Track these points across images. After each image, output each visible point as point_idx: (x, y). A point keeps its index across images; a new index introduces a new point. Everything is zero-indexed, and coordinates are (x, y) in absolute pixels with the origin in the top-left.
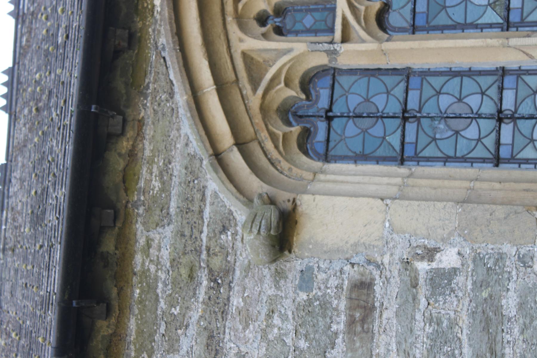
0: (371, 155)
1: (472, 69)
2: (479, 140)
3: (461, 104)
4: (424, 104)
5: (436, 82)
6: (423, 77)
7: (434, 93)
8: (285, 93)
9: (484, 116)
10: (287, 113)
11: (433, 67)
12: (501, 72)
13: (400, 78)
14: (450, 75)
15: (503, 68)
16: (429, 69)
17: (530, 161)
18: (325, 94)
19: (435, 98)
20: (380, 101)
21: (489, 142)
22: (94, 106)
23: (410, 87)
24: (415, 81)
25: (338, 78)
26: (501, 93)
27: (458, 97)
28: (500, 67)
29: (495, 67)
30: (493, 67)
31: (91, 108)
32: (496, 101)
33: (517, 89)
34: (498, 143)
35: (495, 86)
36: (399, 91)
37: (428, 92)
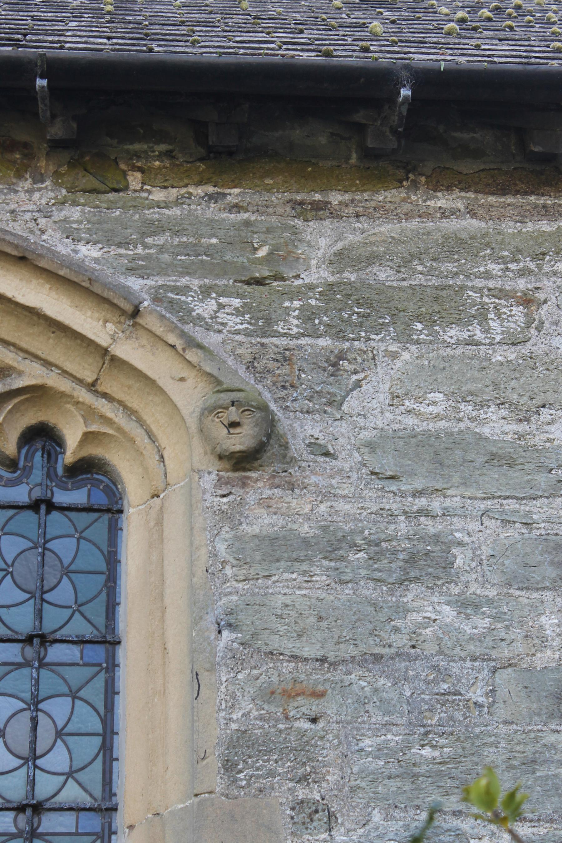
1: (117, 668)
4: (53, 671)
5: (95, 691)
6: (105, 665)
7: (74, 689)
9: (42, 264)
11: (121, 611)
12: (108, 805)
13: (98, 791)
14: (105, 715)
15: (116, 810)
16: (121, 529)
18: (78, 497)
19: (66, 690)
22: (45, 82)
23: (82, 814)
24: (97, 653)
25: (106, 517)
26: (71, 809)
27: (66, 730)
28: (117, 805)
29: (118, 792)
30: (121, 626)
31: (42, 77)
32: (58, 799)
33: (77, 834)
36: (72, 793)
37: (76, 675)
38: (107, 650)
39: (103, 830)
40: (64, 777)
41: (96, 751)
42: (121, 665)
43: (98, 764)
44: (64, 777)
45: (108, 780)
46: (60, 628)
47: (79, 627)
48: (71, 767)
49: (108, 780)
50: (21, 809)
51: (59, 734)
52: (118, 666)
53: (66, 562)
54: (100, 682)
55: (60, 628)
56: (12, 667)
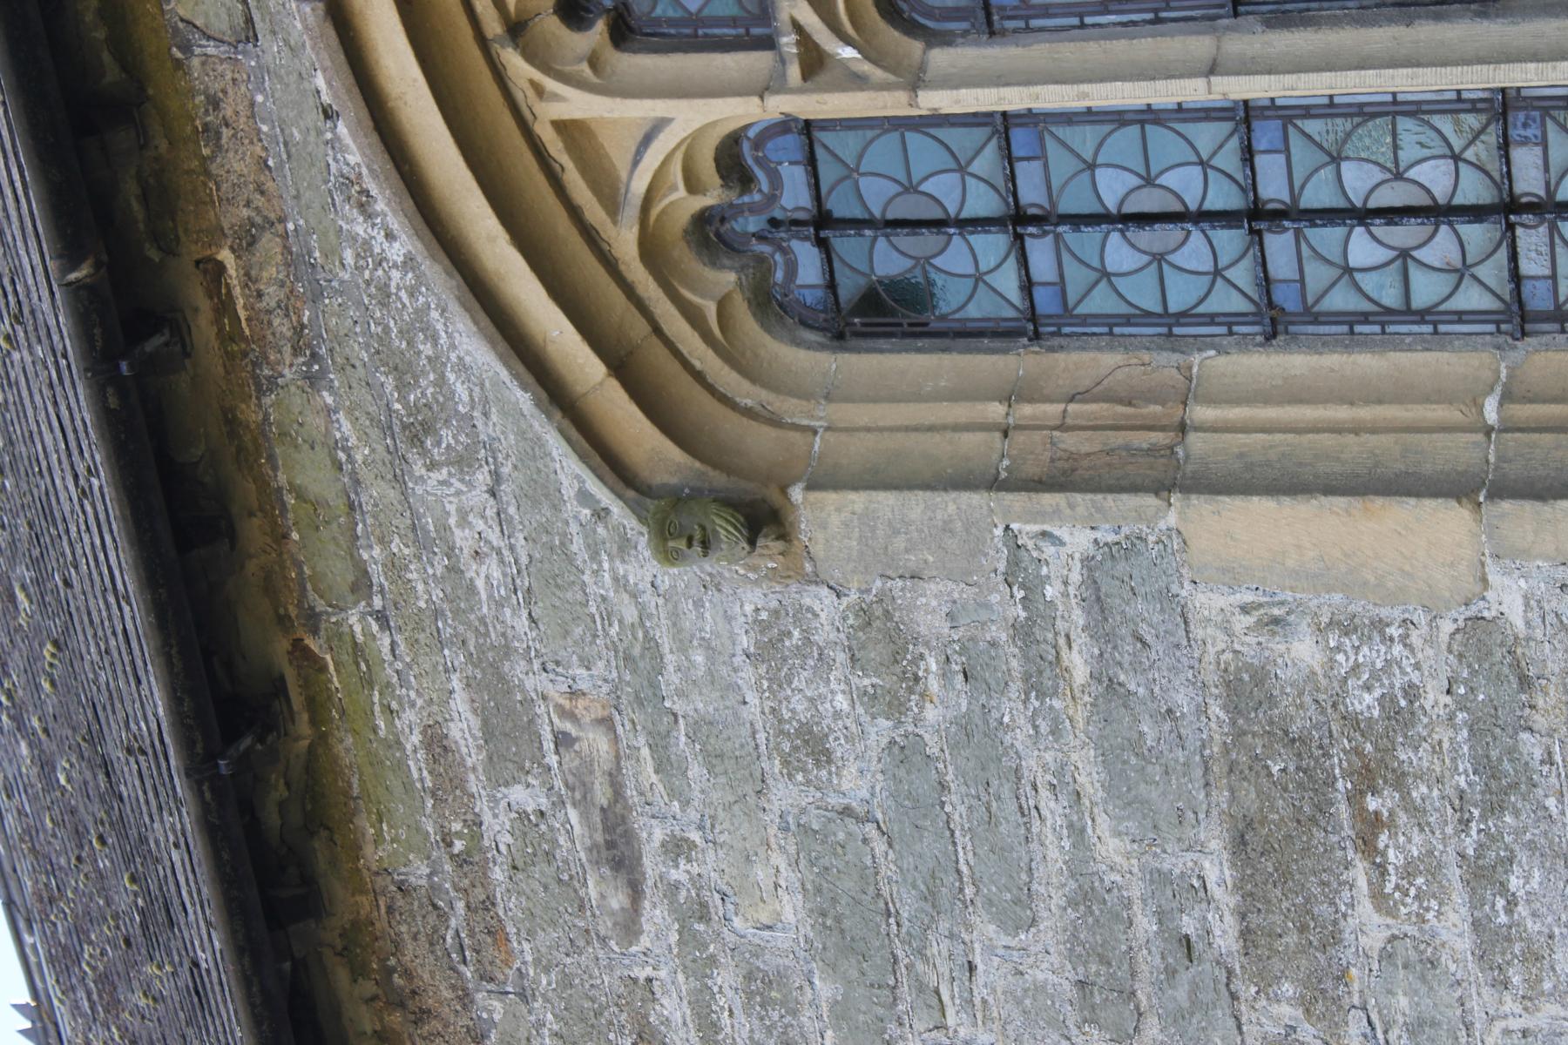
0: (957, 316)
2: (1217, 273)
3: (912, 198)
4: (1303, 187)
5: (1084, 139)
8: (682, 204)
10: (709, 234)
12: (999, 120)
17: (1322, 319)
20: (945, 191)
21: (1242, 275)
34: (1516, 277)
35: (1234, 143)
38: (1257, 117)
39: (1279, 117)
40: (968, 178)
41: (1172, 135)
42: (1180, 99)
43: (1188, 129)
44: (968, 178)
45: (1202, 115)
46: (1491, 177)
47: (987, 162)
48: (1443, 157)
49: (1202, 115)
50: (1019, 238)
51: (1149, 181)
52: (1179, 104)
53: (1136, 181)
54: (1313, 126)
55: (1491, 177)
56: (1304, 246)
